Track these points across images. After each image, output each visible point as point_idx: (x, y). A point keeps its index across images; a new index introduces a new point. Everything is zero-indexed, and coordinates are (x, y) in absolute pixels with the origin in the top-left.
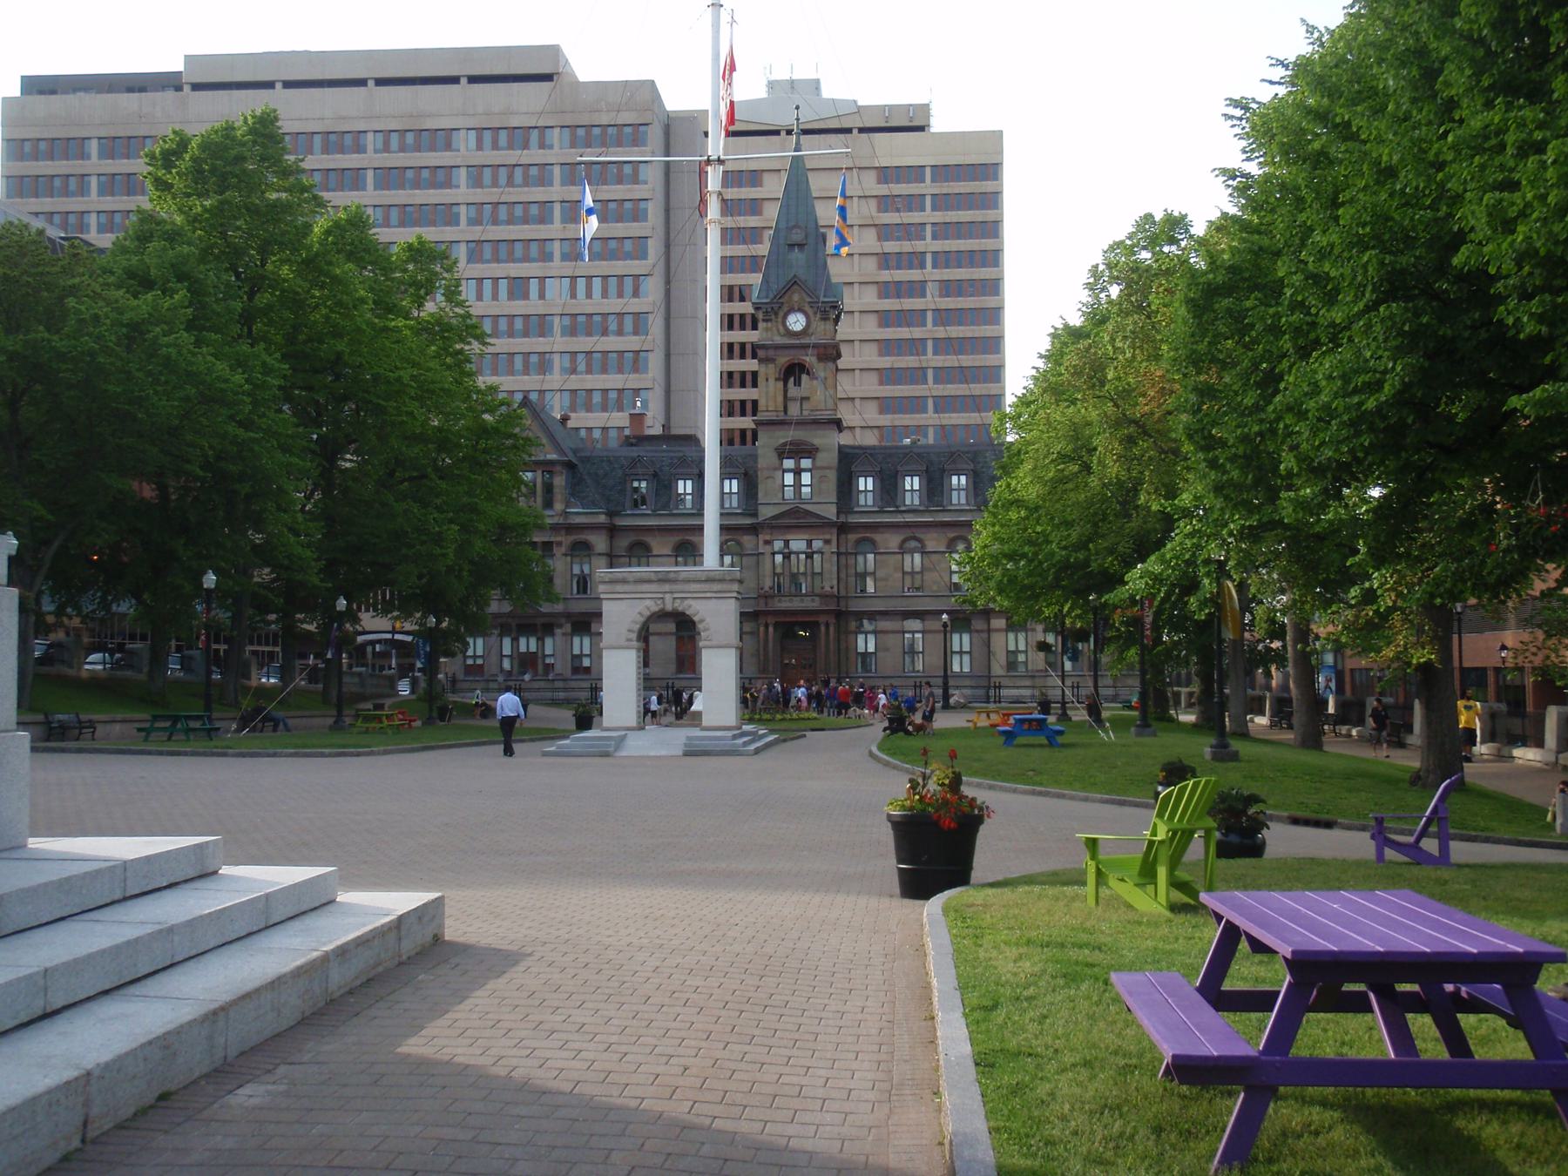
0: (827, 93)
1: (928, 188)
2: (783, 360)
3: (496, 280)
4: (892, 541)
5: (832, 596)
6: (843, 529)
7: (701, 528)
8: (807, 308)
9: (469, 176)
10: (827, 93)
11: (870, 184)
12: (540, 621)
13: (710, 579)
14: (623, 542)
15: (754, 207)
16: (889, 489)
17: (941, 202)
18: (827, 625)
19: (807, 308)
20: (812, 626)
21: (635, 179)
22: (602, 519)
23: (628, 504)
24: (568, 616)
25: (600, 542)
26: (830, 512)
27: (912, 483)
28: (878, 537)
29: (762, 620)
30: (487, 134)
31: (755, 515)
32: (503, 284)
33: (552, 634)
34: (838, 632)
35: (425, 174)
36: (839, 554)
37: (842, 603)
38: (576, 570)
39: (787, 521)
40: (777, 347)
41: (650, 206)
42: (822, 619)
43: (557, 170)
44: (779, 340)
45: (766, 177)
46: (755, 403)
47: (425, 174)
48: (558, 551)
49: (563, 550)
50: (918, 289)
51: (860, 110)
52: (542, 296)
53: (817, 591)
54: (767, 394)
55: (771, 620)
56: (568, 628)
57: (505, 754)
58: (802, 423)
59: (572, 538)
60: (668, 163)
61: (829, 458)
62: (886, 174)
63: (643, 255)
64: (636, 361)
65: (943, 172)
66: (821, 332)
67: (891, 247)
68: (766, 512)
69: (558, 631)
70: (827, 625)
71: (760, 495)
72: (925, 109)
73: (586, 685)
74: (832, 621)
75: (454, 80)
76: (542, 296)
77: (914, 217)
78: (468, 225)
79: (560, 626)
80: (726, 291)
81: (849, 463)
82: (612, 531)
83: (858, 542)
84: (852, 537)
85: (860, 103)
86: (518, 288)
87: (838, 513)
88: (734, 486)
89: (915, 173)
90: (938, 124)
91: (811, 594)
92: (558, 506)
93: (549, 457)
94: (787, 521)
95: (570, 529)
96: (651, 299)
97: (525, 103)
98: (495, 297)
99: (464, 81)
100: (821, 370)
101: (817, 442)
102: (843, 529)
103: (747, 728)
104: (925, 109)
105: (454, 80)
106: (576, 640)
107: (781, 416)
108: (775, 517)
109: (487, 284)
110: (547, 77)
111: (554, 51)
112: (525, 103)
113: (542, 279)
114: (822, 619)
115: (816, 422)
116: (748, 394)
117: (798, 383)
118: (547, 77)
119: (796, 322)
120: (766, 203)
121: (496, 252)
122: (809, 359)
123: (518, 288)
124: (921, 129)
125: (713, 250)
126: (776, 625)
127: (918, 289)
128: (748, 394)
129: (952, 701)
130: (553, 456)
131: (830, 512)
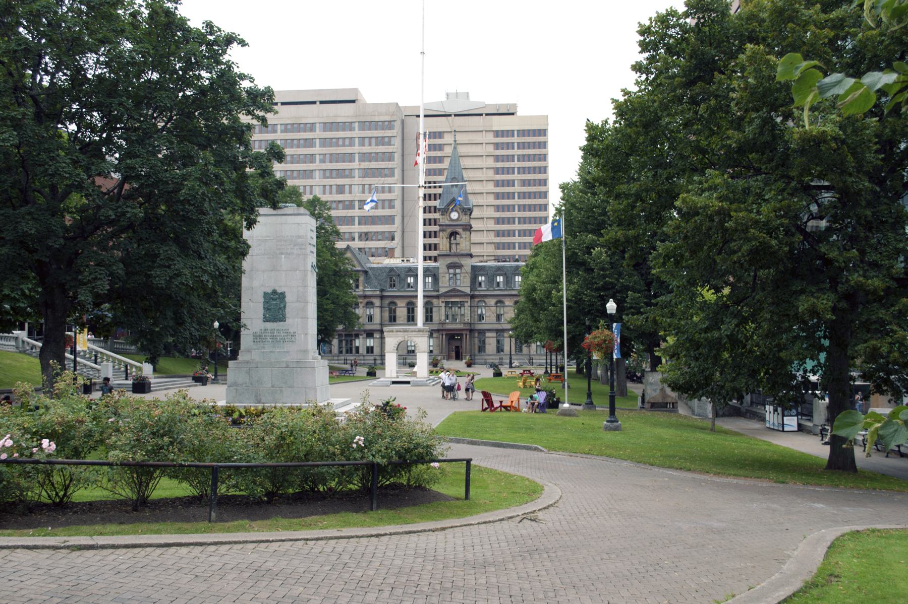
0: (473, 98)
1: (516, 139)
2: (449, 230)
3: (331, 186)
4: (492, 302)
5: (468, 323)
6: (472, 297)
7: (416, 297)
8: (458, 210)
9: (320, 143)
10: (473, 98)
11: (491, 138)
12: (353, 333)
13: (420, 331)
14: (387, 302)
15: (440, 160)
16: (491, 280)
17: (521, 146)
18: (466, 335)
19: (458, 210)
20: (461, 335)
21: (389, 144)
22: (378, 293)
23: (388, 286)
24: (365, 331)
25: (377, 302)
26: (467, 290)
27: (500, 279)
28: (486, 300)
29: (441, 333)
30: (329, 126)
31: (438, 291)
32: (334, 188)
33: (359, 338)
34: (471, 337)
35: (302, 142)
36: (471, 306)
37: (472, 326)
38: (368, 313)
39: (450, 294)
40: (447, 225)
41: (395, 123)
42: (464, 332)
43: (357, 140)
44: (447, 223)
45: (446, 135)
46: (435, 245)
47: (302, 142)
48: (361, 306)
49: (363, 305)
50: (511, 183)
51: (486, 106)
52: (350, 193)
53: (463, 321)
54: (442, 241)
55: (444, 333)
56: (365, 335)
57: (282, 296)
58: (456, 255)
59: (366, 300)
60: (403, 187)
61: (469, 269)
62: (497, 134)
63: (392, 175)
64: (390, 157)
65: (523, 133)
66: (465, 220)
67: (500, 165)
68: (442, 290)
69: (361, 337)
70: (466, 335)
71: (440, 283)
72: (515, 106)
73: (372, 358)
74: (468, 333)
75: (314, 103)
76: (350, 193)
77: (510, 152)
78: (320, 162)
79: (362, 335)
80: (413, 320)
81: (476, 271)
82: (382, 298)
83: (479, 301)
84: (477, 300)
85: (486, 103)
86: (341, 189)
87: (471, 290)
88: (430, 280)
89: (510, 133)
90: (520, 113)
91: (460, 323)
92: (361, 288)
93: (357, 269)
94: (450, 294)
95: (365, 297)
96: (396, 194)
97: (343, 113)
98: (331, 193)
99: (318, 103)
100: (464, 234)
101: (462, 262)
102: (472, 297)
103: (431, 377)
104: (515, 106)
105: (314, 103)
106: (368, 340)
107: (448, 252)
108: (446, 292)
109: (328, 187)
110: (353, 101)
111: (356, 91)
112: (343, 113)
113: (350, 186)
114: (464, 332)
115: (463, 255)
116: (433, 241)
117: (455, 239)
118: (353, 101)
119: (454, 215)
120: (445, 134)
121: (331, 174)
122: (460, 230)
123: (341, 189)
124: (513, 114)
125: (422, 166)
126: (446, 335)
127: (511, 183)
128: (433, 241)
129: (513, 365)
130: (359, 268)
131: (467, 290)
